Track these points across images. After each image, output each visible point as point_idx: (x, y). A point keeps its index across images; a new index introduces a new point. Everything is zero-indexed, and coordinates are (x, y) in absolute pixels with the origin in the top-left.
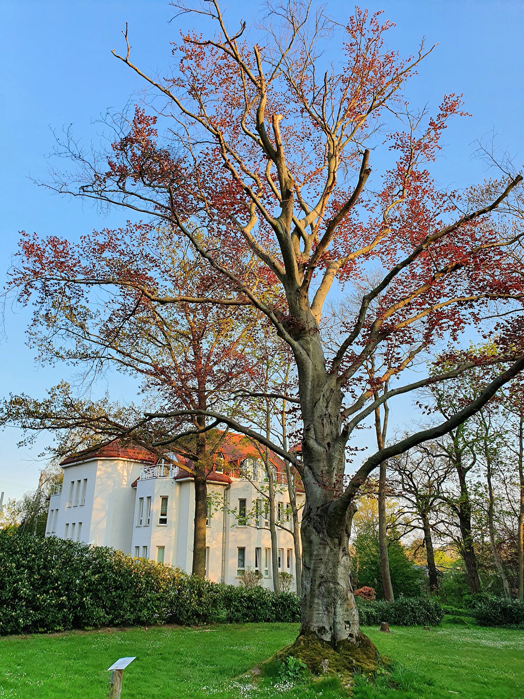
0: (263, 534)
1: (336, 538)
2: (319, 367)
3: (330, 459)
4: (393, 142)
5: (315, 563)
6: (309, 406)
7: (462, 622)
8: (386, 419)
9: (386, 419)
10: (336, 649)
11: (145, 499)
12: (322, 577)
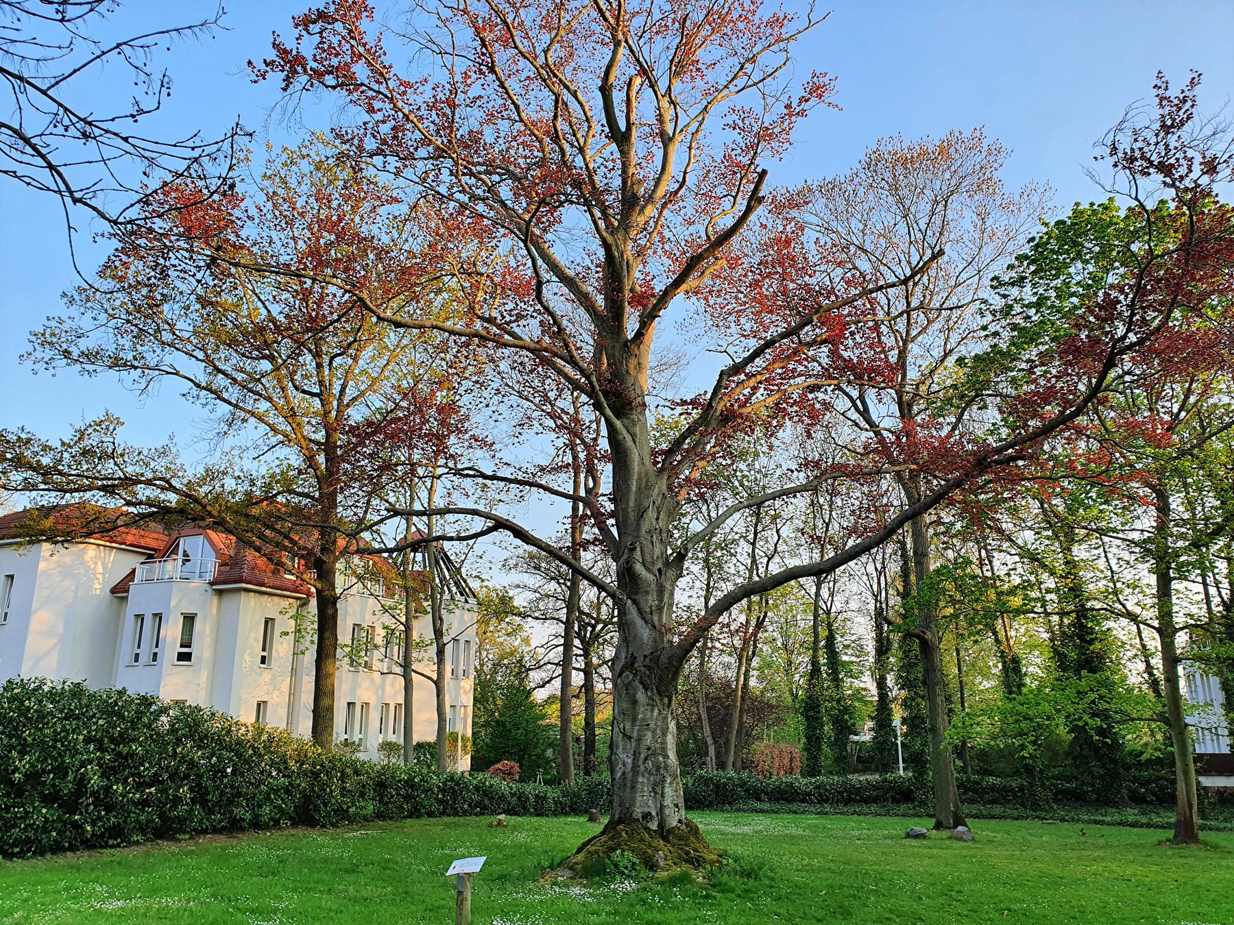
0: (359, 679)
2: (648, 461)
3: (661, 590)
4: (729, 120)
6: (632, 515)
10: (665, 839)
12: (649, 749)
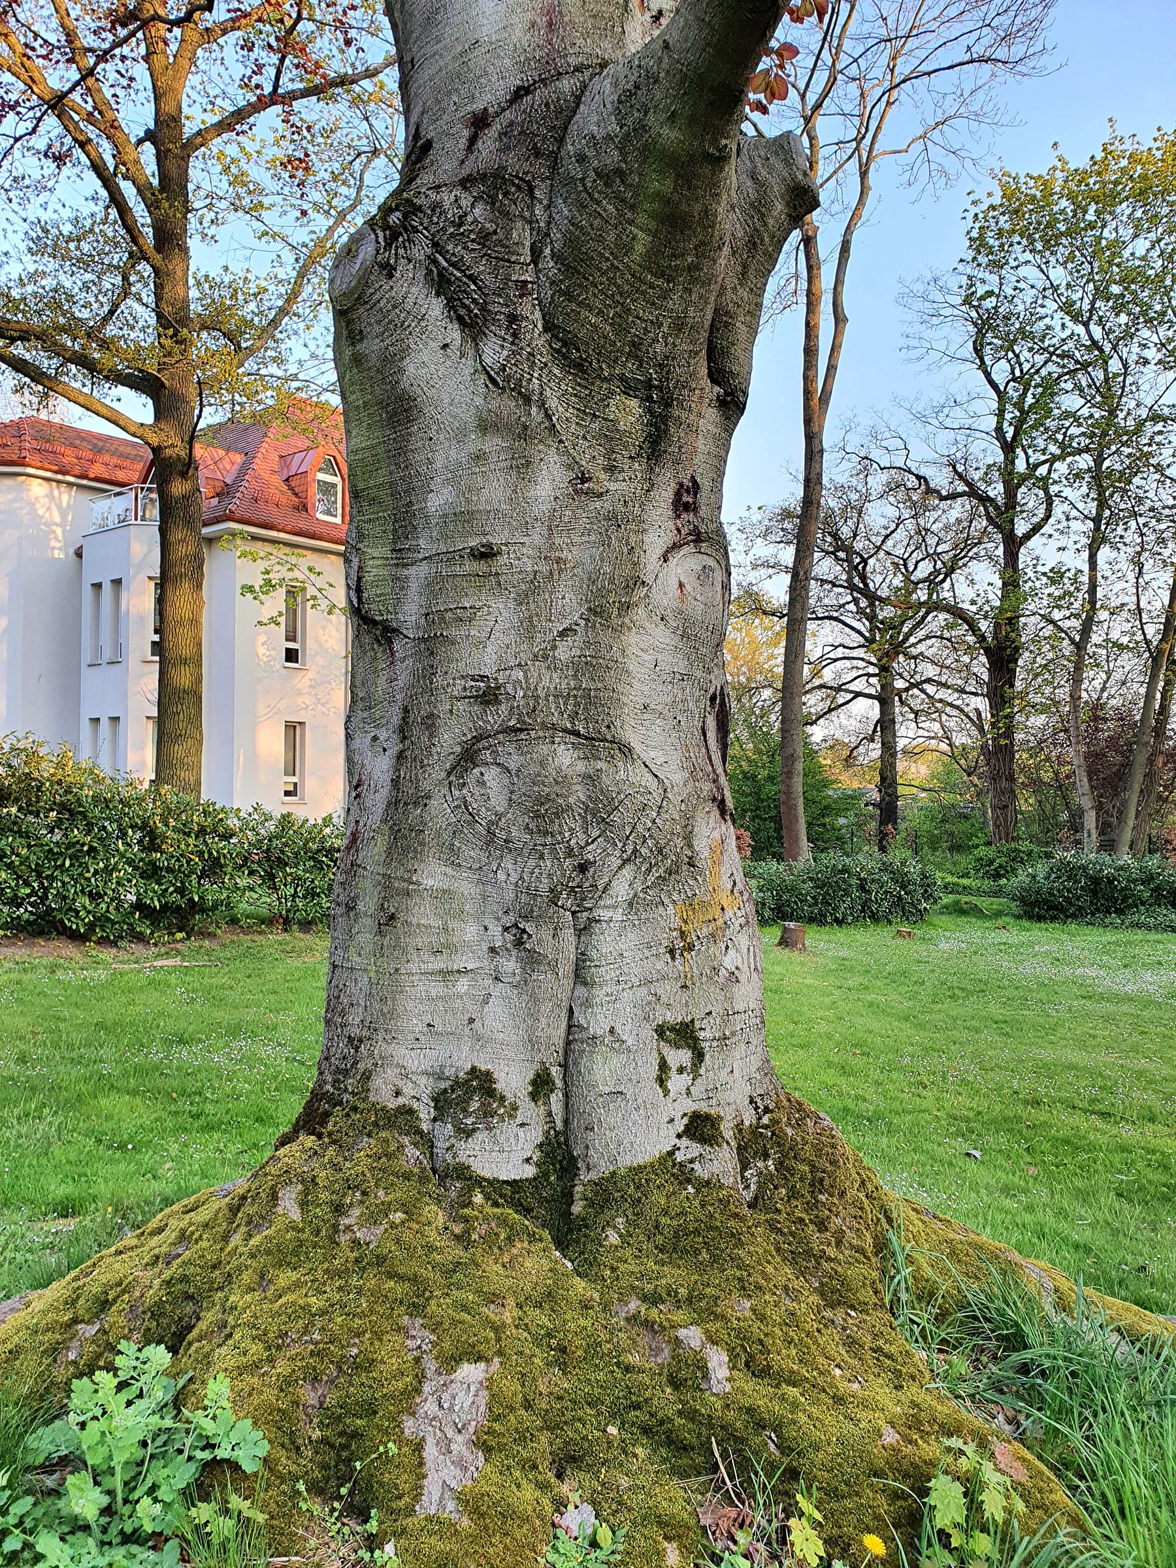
1: (629, 388)
5: (434, 587)
7: (973, 911)
8: (835, 349)
9: (835, 349)
10: (568, 1234)
11: (107, 588)
12: (489, 697)
